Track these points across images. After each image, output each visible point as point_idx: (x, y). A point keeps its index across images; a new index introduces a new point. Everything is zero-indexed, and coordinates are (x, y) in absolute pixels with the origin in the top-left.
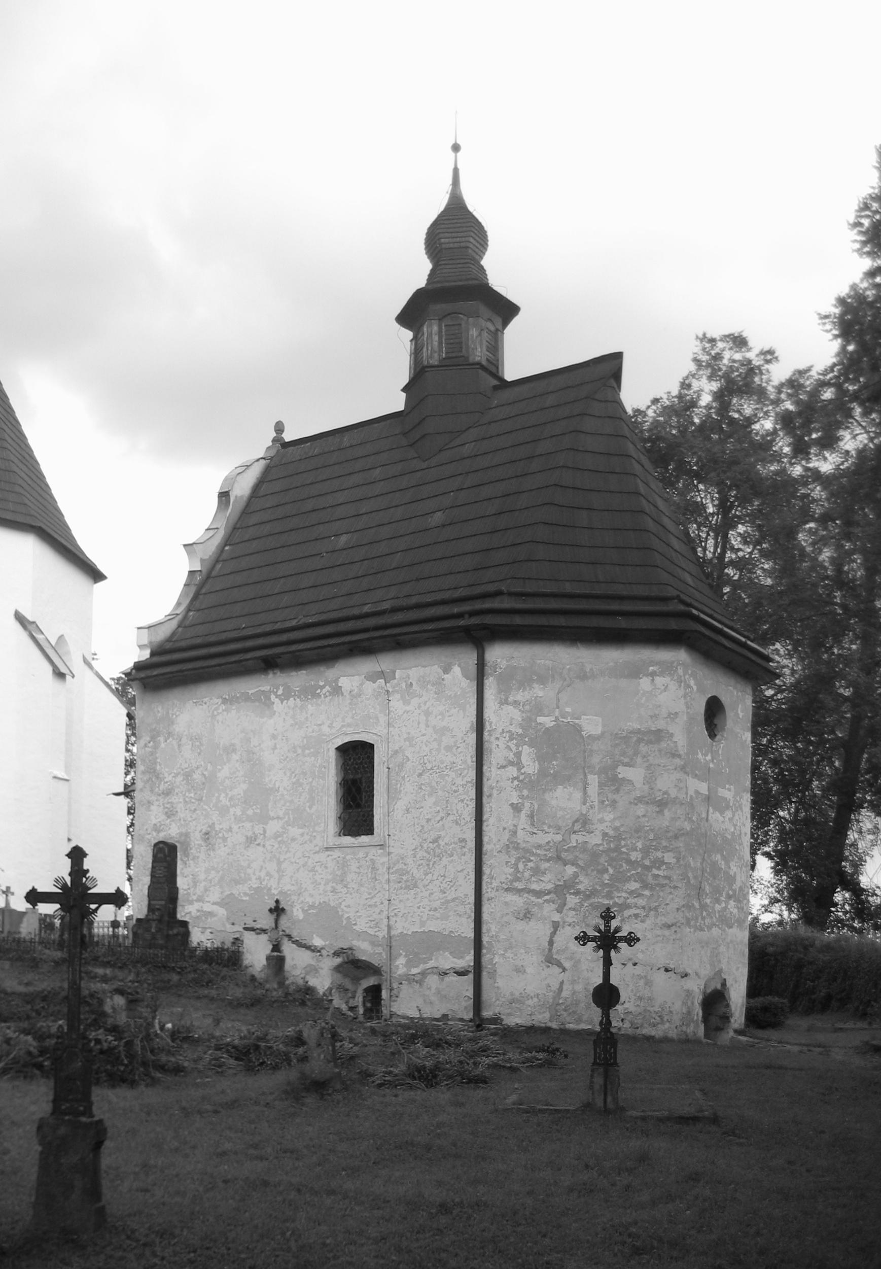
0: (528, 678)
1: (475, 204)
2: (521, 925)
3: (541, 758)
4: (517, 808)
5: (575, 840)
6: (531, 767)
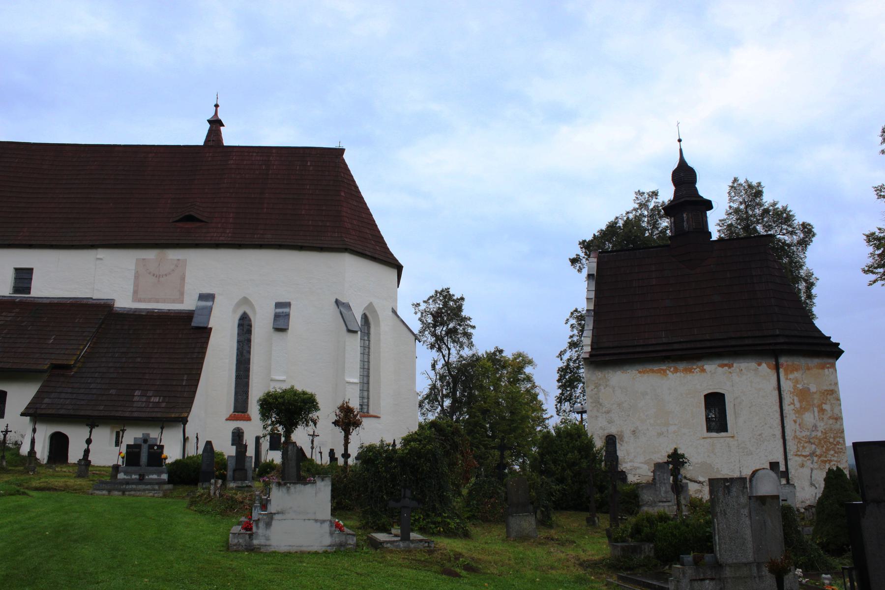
0: (796, 369)
1: (690, 163)
2: (801, 470)
3: (800, 401)
4: (795, 422)
5: (814, 434)
6: (798, 405)
